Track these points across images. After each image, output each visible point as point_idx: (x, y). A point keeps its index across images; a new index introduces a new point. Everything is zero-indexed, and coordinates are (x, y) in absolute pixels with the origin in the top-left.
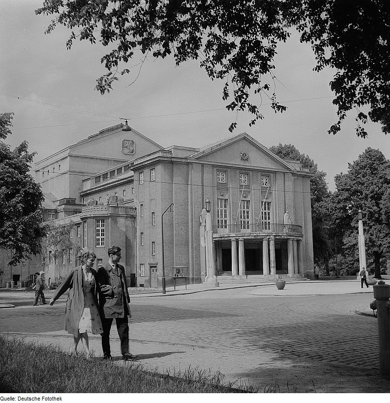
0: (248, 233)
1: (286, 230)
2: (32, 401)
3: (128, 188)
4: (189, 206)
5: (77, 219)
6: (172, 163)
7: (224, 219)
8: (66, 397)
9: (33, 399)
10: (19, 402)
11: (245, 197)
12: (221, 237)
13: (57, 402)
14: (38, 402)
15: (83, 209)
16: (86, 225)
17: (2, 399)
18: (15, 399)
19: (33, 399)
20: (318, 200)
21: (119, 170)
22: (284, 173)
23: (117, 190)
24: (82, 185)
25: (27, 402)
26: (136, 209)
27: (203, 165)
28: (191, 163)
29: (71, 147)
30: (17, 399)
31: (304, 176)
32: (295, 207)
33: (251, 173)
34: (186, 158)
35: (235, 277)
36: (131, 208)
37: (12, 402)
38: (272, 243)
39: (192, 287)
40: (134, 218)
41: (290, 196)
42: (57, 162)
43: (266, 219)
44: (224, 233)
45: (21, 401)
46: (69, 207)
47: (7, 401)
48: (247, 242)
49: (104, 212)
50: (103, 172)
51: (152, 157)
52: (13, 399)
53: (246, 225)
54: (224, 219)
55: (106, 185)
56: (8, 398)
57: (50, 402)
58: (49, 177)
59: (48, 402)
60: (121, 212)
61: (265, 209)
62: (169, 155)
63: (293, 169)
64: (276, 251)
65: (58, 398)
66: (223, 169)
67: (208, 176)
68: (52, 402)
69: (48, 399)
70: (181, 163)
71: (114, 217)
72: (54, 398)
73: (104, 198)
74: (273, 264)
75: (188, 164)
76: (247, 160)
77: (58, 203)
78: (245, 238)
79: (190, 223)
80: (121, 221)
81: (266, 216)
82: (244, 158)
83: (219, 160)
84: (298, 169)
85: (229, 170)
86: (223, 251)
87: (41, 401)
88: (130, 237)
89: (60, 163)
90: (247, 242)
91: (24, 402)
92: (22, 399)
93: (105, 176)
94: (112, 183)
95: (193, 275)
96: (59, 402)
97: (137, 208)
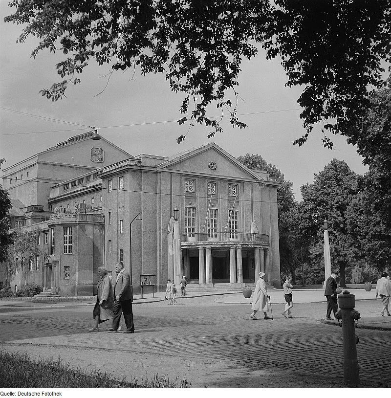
0: (215, 241)
1: (253, 239)
2: (31, 396)
3: (96, 196)
4: (158, 214)
5: (44, 226)
6: (141, 171)
7: (191, 227)
8: (66, 392)
9: (33, 394)
10: (19, 397)
11: (213, 206)
12: (189, 246)
13: (56, 397)
14: (37, 397)
15: (51, 216)
16: (54, 232)
17: (2, 394)
18: (15, 394)
19: (33, 394)
20: (285, 209)
21: (88, 178)
22: (252, 183)
23: (85, 197)
24: (50, 193)
25: (27, 397)
26: (104, 216)
27: (171, 174)
28: (160, 172)
29: (39, 155)
30: (16, 394)
31: (271, 186)
32: (262, 216)
33: (219, 182)
34: (154, 167)
35: (202, 286)
36: (99, 216)
37: (12, 397)
38: (239, 252)
39: (160, 295)
40: (102, 225)
41: (257, 206)
42: (25, 169)
43: (233, 228)
44: (192, 241)
45: (21, 396)
46: (36, 214)
47: (7, 396)
48: (214, 251)
49: (73, 220)
50: (71, 179)
51: (121, 165)
52: (13, 394)
53: (214, 234)
54: (191, 227)
55: (74, 192)
56: (8, 393)
57: (49, 397)
58: (17, 184)
59: (47, 397)
60: (89, 219)
61: (233, 218)
62: (137, 164)
63: (260, 179)
64: (243, 259)
65: (58, 393)
66: (191, 178)
67: (176, 185)
68: (52, 397)
69: (48, 394)
70: (150, 172)
71: (82, 225)
72: (53, 393)
73: (72, 206)
74: (240, 273)
75: (157, 172)
76: (215, 169)
77: (26, 210)
78: (212, 246)
79: (158, 231)
80: (89, 229)
81: (234, 225)
82: (213, 167)
83: (188, 169)
84: (265, 179)
85: (197, 179)
86: (190, 259)
87: (41, 396)
88: (98, 245)
89: (28, 170)
90: (214, 251)
91: (24, 397)
92: (22, 394)
93: (73, 183)
94: (80, 190)
95: (160, 283)
96: (59, 397)
97: (106, 216)
